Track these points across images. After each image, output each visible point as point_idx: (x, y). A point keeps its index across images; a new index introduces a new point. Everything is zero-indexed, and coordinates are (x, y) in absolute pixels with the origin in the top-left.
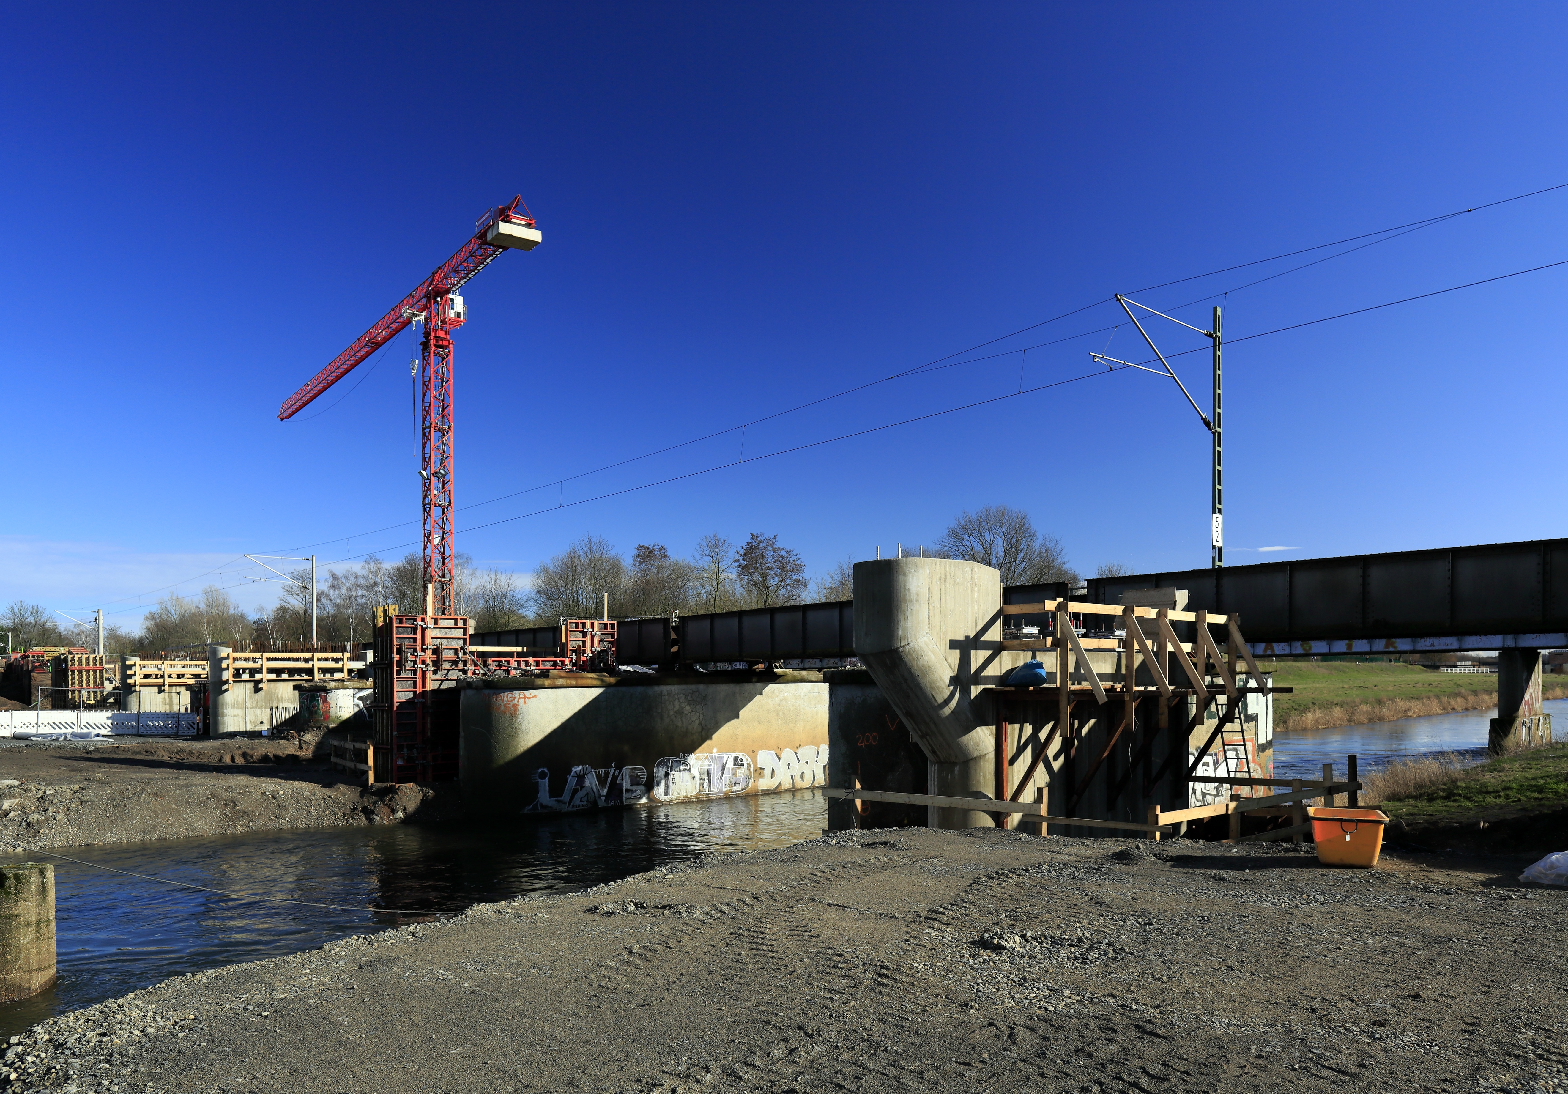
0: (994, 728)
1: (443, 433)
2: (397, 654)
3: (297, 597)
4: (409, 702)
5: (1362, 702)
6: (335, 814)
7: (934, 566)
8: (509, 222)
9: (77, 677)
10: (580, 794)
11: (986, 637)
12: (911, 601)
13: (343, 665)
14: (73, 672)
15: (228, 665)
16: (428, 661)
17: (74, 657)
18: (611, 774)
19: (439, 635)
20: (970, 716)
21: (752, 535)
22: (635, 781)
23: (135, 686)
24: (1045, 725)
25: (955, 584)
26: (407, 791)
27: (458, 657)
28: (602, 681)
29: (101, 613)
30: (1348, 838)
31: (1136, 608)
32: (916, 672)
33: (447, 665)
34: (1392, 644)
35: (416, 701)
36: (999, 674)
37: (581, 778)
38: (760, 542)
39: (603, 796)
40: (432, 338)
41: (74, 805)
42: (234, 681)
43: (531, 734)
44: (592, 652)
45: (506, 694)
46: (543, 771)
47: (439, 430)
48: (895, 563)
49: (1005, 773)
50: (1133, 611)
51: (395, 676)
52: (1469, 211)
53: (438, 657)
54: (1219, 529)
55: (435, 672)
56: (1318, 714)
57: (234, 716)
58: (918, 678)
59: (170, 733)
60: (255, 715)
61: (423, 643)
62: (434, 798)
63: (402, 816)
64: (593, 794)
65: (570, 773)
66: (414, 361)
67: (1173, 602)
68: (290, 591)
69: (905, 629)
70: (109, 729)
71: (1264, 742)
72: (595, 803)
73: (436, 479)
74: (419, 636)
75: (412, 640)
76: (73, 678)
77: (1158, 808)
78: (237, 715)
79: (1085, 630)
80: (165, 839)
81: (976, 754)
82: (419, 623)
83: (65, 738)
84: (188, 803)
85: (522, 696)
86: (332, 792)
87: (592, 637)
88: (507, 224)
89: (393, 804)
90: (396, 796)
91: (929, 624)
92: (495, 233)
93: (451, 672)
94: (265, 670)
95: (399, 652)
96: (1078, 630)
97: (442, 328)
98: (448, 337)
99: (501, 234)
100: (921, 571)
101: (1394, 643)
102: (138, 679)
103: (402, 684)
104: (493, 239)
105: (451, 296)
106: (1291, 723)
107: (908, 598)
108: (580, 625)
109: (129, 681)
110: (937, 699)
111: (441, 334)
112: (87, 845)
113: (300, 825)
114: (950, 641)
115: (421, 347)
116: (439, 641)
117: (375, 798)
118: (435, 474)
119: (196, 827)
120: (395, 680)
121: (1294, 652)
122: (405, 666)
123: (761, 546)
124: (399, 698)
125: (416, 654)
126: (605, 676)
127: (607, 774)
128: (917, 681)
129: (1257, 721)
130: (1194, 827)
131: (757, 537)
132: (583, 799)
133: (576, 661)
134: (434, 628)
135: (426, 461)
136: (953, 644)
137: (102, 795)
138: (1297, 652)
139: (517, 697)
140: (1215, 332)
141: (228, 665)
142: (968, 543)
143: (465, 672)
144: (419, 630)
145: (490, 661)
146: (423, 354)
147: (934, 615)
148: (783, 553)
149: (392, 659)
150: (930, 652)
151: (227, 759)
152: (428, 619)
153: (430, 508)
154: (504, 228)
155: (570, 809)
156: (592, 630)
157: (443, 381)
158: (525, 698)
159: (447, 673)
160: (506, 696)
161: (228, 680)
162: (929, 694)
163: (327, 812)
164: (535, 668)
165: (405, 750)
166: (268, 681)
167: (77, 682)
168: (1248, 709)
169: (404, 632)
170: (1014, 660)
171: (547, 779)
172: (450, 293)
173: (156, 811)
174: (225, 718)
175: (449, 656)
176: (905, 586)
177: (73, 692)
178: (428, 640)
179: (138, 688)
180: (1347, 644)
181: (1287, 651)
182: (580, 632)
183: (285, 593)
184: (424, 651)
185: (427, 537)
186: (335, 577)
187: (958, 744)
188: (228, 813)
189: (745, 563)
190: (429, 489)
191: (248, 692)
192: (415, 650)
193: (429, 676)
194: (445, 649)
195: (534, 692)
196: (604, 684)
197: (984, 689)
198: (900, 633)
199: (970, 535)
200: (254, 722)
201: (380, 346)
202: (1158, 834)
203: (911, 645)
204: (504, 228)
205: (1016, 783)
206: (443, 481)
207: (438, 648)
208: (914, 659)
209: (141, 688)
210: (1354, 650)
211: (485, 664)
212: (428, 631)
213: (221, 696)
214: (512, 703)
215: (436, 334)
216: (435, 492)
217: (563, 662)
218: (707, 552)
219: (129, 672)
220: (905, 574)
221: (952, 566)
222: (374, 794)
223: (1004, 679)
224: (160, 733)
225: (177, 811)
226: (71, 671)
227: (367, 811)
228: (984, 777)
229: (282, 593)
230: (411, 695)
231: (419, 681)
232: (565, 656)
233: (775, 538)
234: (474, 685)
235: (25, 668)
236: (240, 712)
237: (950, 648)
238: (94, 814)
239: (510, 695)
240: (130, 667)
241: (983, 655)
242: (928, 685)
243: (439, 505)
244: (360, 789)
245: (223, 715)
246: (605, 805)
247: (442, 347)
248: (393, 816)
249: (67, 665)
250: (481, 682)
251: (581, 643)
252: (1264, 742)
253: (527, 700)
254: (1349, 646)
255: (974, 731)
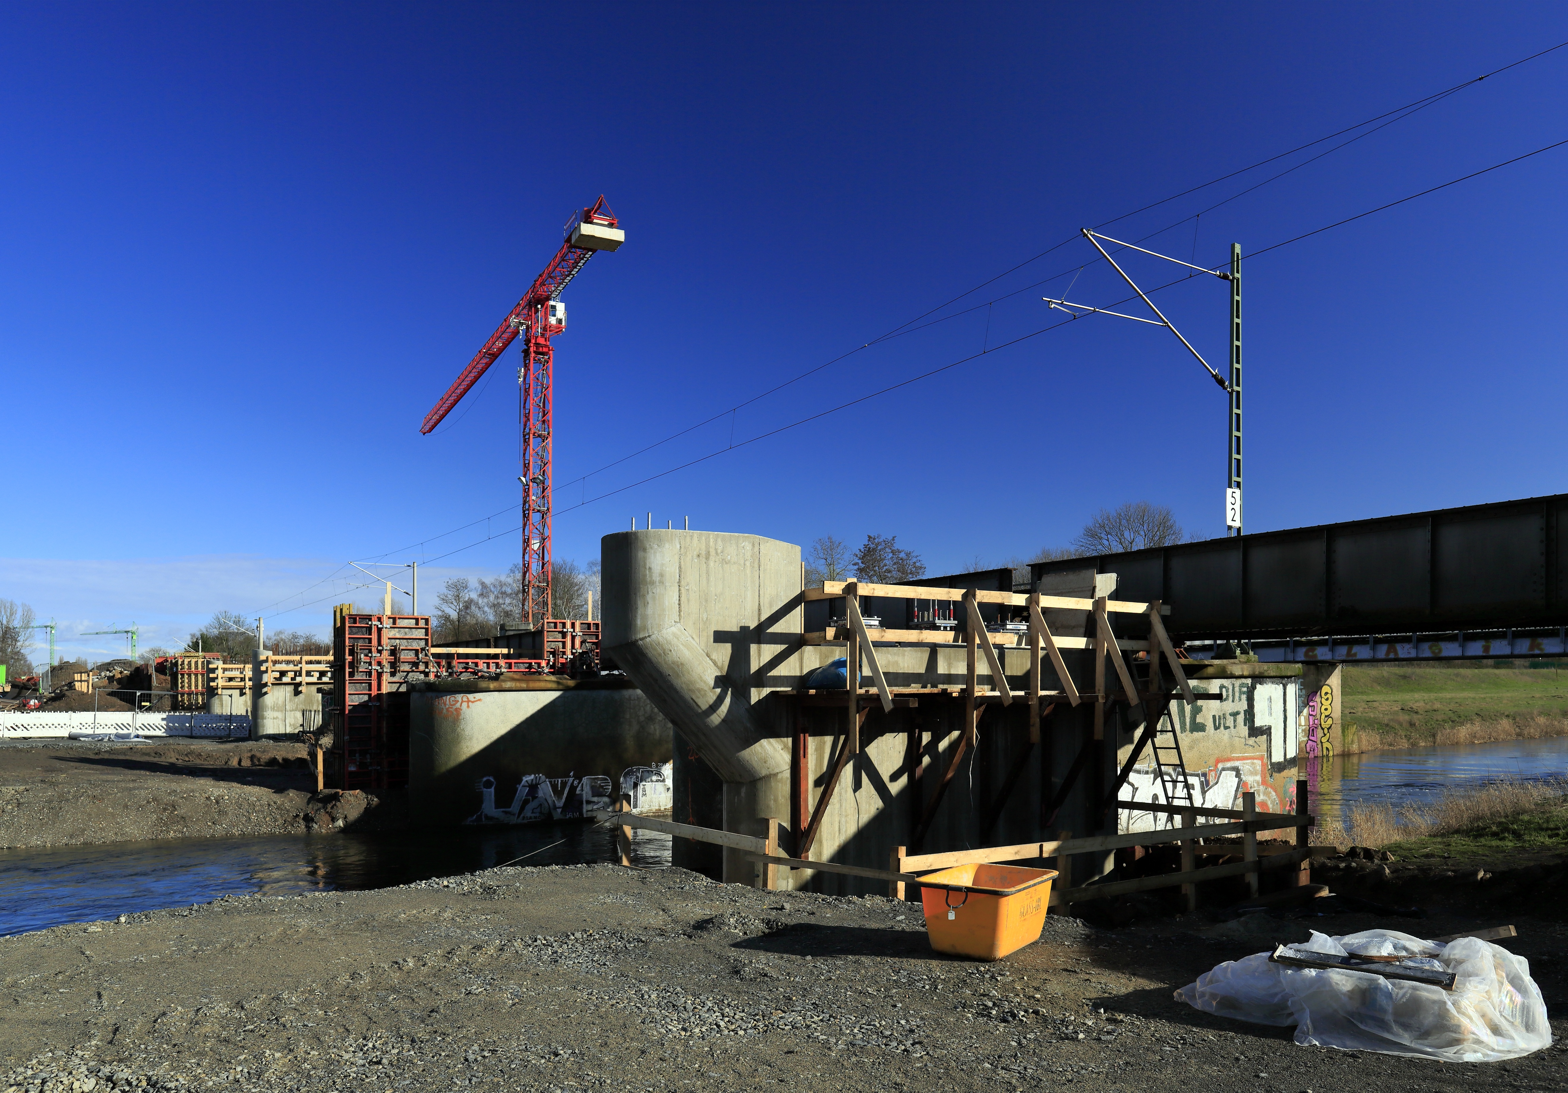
0: (789, 741)
1: (544, 439)
2: (349, 655)
3: (451, 605)
4: (363, 705)
5: (1540, 714)
6: (276, 821)
7: (688, 539)
8: (591, 223)
9: (186, 681)
10: (532, 805)
11: (778, 628)
12: (653, 583)
13: (301, 668)
14: (183, 675)
15: (267, 668)
16: (385, 663)
17: (184, 661)
18: (569, 784)
19: (398, 636)
20: (748, 725)
21: (869, 537)
22: (597, 792)
23: (217, 689)
24: (876, 738)
25: (724, 562)
26: (352, 799)
27: (418, 659)
28: (558, 683)
29: (262, 621)
30: (952, 916)
31: (978, 592)
32: (666, 671)
33: (407, 667)
34: (1538, 646)
35: (370, 704)
36: (798, 674)
37: (533, 787)
38: (878, 544)
39: (559, 808)
40: (532, 345)
41: (10, 807)
42: (273, 684)
43: (474, 740)
44: (573, 654)
45: (448, 697)
46: (488, 781)
47: (539, 436)
48: (633, 537)
49: (802, 796)
50: (974, 596)
51: (347, 678)
52: (1480, 79)
53: (395, 659)
54: (1237, 507)
55: (393, 674)
56: (1477, 727)
57: (274, 718)
58: (669, 678)
59: (223, 734)
60: (295, 718)
61: (380, 644)
62: (378, 806)
63: (342, 825)
64: (546, 805)
65: (520, 783)
66: (521, 370)
67: (1092, 588)
68: (445, 600)
69: (645, 617)
70: (163, 730)
71: (1282, 759)
72: (550, 815)
73: (535, 485)
74: (374, 637)
75: (367, 641)
76: (183, 682)
77: (902, 850)
78: (277, 718)
79: (956, 622)
80: (91, 843)
81: (764, 773)
82: (374, 623)
83: (110, 738)
84: (126, 806)
85: (465, 699)
86: (281, 797)
87: (573, 638)
88: (589, 225)
89: (334, 811)
90: (338, 804)
91: (680, 611)
92: (577, 235)
93: (410, 674)
94: (304, 673)
95: (352, 652)
96: (947, 621)
97: (543, 335)
98: (548, 343)
99: (583, 235)
100: (667, 545)
101: (1539, 644)
102: (221, 682)
103: (355, 687)
104: (576, 241)
105: (552, 303)
106: (1439, 738)
107: (648, 579)
108: (560, 626)
109: (212, 684)
110: (700, 704)
111: (541, 341)
112: (9, 848)
113: (236, 832)
114: (715, 632)
115: (523, 354)
116: (398, 641)
117: (320, 805)
118: (534, 480)
119: (127, 832)
120: (347, 682)
121: (1421, 655)
122: (358, 668)
123: (879, 548)
124: (352, 701)
125: (370, 655)
126: (566, 679)
127: (564, 784)
128: (670, 681)
129: (1270, 735)
130: (1124, 865)
131: (874, 539)
132: (535, 811)
133: (554, 663)
134: (391, 628)
135: (526, 466)
136: (720, 637)
137: (41, 797)
138: (1424, 656)
139: (460, 701)
140: (1232, 274)
141: (267, 668)
142: (1106, 543)
143: (427, 674)
144: (374, 630)
145: (454, 663)
146: (525, 361)
147: (688, 600)
148: (902, 555)
149: (345, 659)
150: (681, 646)
151: (234, 763)
152: (385, 619)
153: (529, 514)
154: (586, 229)
155: (520, 821)
156: (572, 630)
157: (543, 387)
158: (468, 701)
159: (407, 675)
160: (448, 699)
161: (267, 683)
162: (687, 697)
163: (268, 819)
164: (506, 670)
165: (357, 755)
166: (308, 684)
167: (186, 685)
168: (1255, 720)
169: (359, 631)
170: (822, 657)
171: (493, 789)
172: (551, 299)
173: (90, 815)
174: (265, 721)
175: (409, 657)
176: (645, 564)
177: (183, 695)
178: (385, 641)
179: (220, 691)
180: (1484, 646)
181: (1413, 654)
182: (559, 632)
183: (441, 602)
184: (380, 652)
185: (526, 542)
186: (483, 585)
187: (739, 760)
188: (164, 818)
189: (862, 566)
190: (528, 495)
191: (288, 695)
192: (370, 651)
193: (386, 678)
194: (402, 650)
195: (478, 696)
196: (561, 687)
197: (772, 692)
198: (639, 622)
199: (1108, 533)
200: (294, 725)
201: (497, 357)
202: (901, 886)
203: (653, 637)
204: (586, 229)
205: (811, 809)
206: (543, 487)
207: (395, 649)
208: (660, 655)
209: (224, 690)
210: (1491, 653)
211: (449, 666)
212: (384, 631)
213: (261, 699)
214: (454, 707)
215: (536, 341)
216: (534, 498)
217: (539, 665)
218: (821, 555)
219: (211, 675)
220: (645, 550)
221: (719, 540)
222: (319, 800)
223: (803, 682)
224: (213, 734)
225: (113, 815)
226: (181, 674)
227: (308, 819)
228: (776, 800)
229: (437, 601)
230: (366, 698)
231: (374, 684)
232: (542, 658)
233: (893, 540)
234: (417, 688)
235: (145, 672)
236: (279, 715)
237: (715, 641)
238: (27, 816)
239: (453, 699)
240: (213, 670)
241: (769, 651)
242: (684, 686)
243: (539, 511)
244: (309, 795)
245: (263, 718)
246: (561, 817)
247: (543, 354)
248: (333, 825)
249: (177, 669)
250: (423, 685)
251: (560, 645)
252: (1282, 759)
253: (470, 703)
254: (1487, 649)
255: (757, 744)
